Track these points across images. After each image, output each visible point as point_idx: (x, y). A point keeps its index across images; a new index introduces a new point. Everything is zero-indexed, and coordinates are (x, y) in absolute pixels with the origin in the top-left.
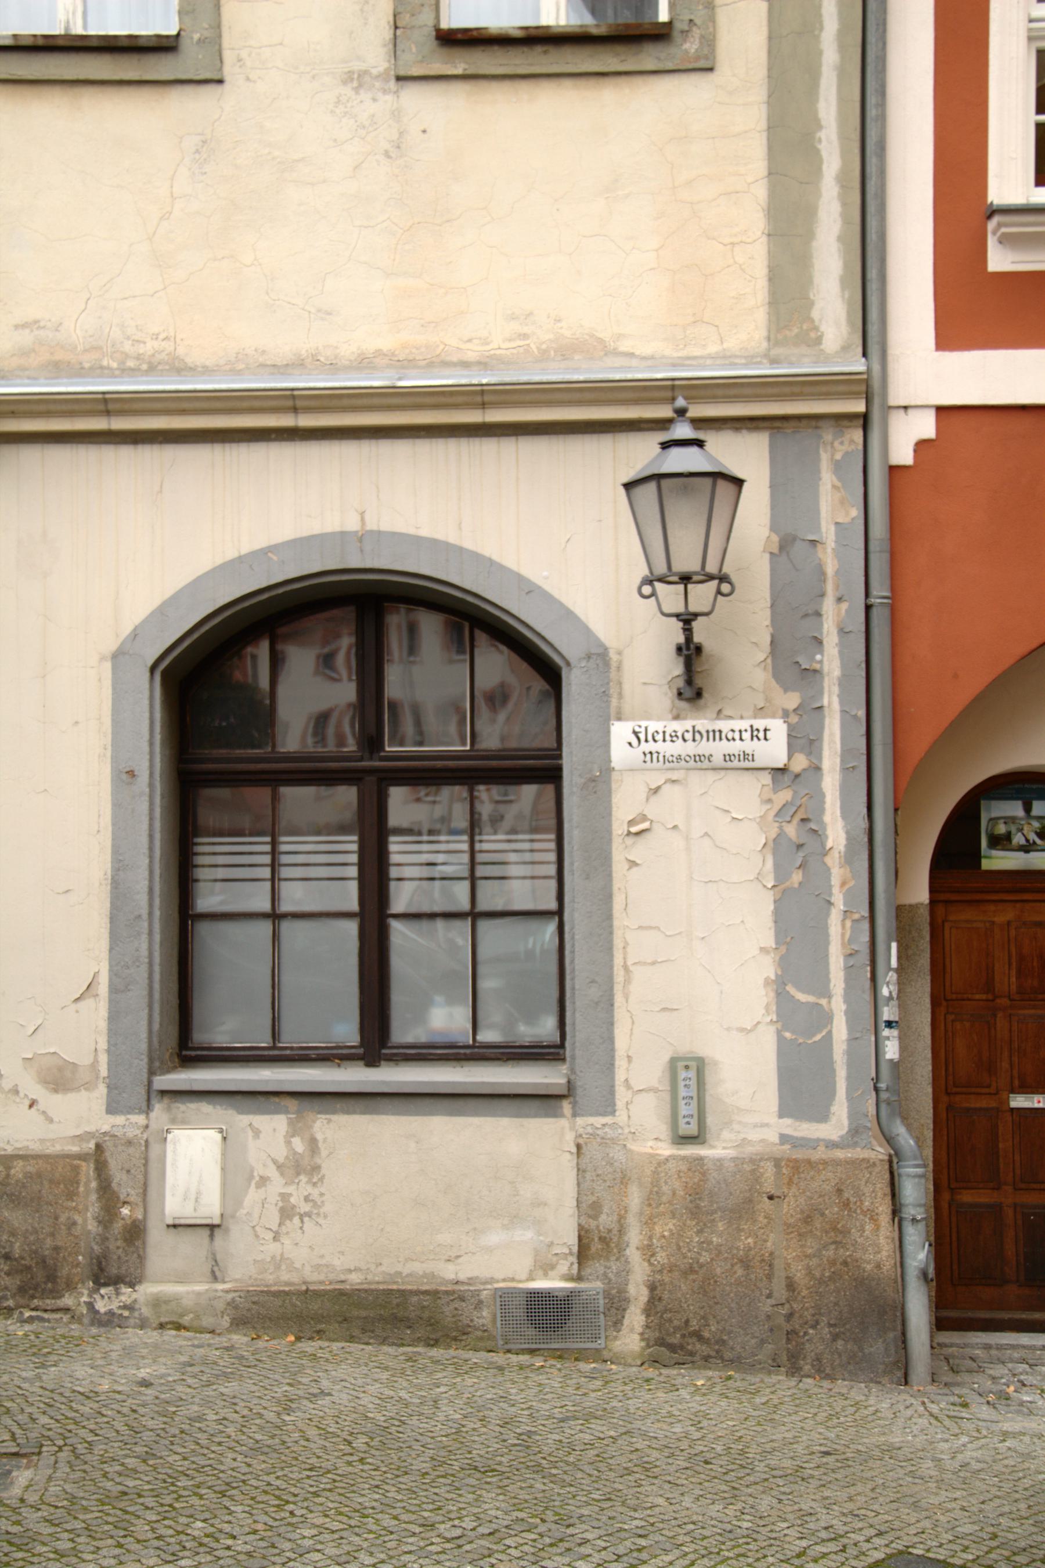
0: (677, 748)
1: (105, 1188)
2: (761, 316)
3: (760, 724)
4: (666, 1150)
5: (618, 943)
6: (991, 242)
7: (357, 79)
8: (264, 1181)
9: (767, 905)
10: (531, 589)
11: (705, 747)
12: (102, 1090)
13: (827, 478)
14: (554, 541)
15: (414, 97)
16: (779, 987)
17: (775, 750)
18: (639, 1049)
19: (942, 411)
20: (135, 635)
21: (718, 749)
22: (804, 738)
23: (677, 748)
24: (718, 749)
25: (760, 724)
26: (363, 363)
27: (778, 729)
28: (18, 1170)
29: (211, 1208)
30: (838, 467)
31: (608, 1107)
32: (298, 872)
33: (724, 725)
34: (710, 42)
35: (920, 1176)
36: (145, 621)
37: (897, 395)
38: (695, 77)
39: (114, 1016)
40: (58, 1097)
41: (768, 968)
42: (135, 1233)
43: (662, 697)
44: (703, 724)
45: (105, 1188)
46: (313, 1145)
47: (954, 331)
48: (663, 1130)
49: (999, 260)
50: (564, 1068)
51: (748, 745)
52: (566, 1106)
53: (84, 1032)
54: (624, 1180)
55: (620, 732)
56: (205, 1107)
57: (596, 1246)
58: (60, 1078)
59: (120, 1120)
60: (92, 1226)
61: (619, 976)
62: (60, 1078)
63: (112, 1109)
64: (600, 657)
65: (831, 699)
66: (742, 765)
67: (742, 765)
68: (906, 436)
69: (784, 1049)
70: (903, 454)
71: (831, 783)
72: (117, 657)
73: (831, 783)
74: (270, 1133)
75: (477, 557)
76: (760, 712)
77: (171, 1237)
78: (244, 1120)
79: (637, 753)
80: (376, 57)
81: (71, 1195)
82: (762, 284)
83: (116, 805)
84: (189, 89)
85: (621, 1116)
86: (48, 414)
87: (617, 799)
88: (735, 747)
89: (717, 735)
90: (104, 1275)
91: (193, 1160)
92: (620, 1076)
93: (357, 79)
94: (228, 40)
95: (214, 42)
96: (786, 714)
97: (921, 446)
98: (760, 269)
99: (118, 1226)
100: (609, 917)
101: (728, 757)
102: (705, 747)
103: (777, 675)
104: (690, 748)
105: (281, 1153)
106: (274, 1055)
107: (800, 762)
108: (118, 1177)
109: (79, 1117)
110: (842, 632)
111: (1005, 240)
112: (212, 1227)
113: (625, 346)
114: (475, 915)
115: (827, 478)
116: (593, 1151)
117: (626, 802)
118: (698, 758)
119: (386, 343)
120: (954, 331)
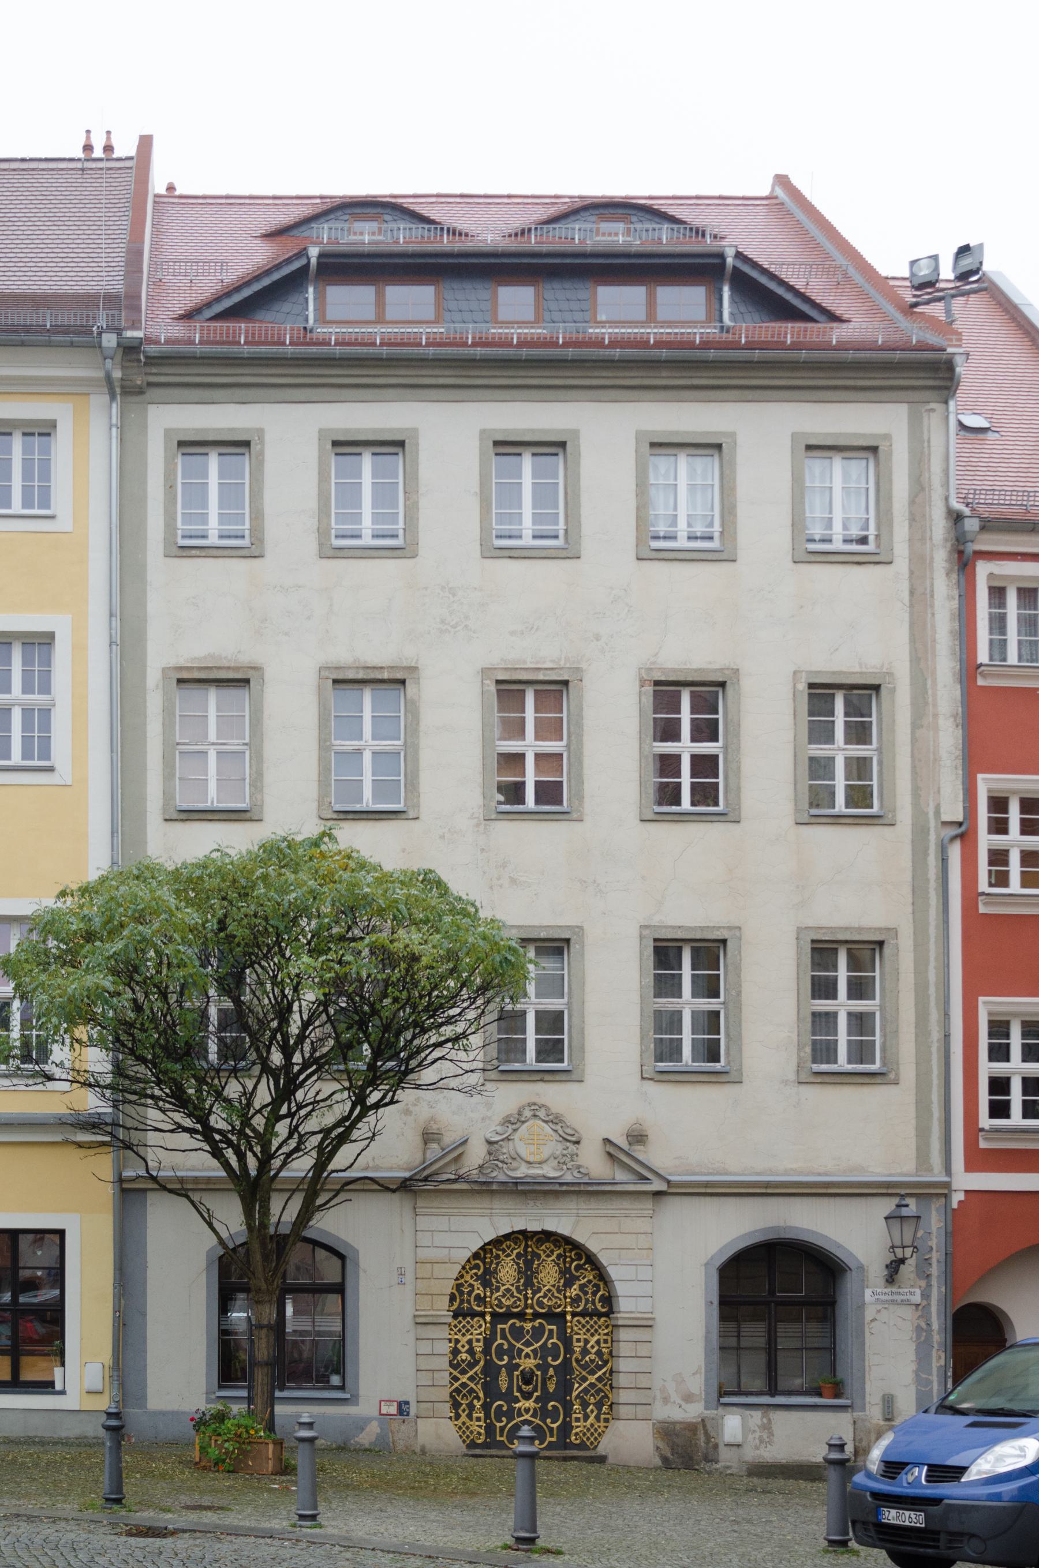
0: (886, 1297)
1: (706, 1433)
2: (914, 1161)
3: (912, 1290)
4: (882, 1423)
5: (867, 1358)
6: (980, 1139)
7: (785, 1082)
8: (754, 1431)
9: (913, 1346)
10: (839, 1246)
11: (895, 1297)
12: (703, 1403)
13: (934, 1213)
14: (856, 1235)
15: (803, 1087)
16: (917, 1373)
17: (917, 1298)
18: (873, 1393)
19: (966, 1191)
20: (712, 1258)
21: (899, 1298)
22: (926, 1296)
23: (886, 1297)
24: (899, 1298)
25: (912, 1290)
26: (786, 1173)
27: (918, 1291)
28: (678, 1427)
29: (739, 1439)
30: (937, 1210)
31: (863, 1409)
32: (783, 1334)
33: (901, 1290)
34: (897, 1075)
35: (619, 1312)
36: (716, 1254)
37: (954, 1187)
38: (893, 1086)
39: (706, 1380)
40: (689, 1405)
41: (913, 1367)
42: (716, 1446)
43: (882, 1281)
44: (894, 1290)
45: (706, 1433)
46: (769, 1420)
47: (971, 1166)
48: (880, 1417)
49: (983, 1145)
50: (440, 1432)
51: (909, 1297)
52: (850, 1410)
53: (697, 1384)
54: (870, 1432)
55: (868, 1293)
56: (735, 1409)
57: (861, 1452)
58: (689, 1398)
59: (709, 1412)
60: (703, 1444)
61: (867, 1369)
62: (689, 1398)
63: (706, 1408)
64: (861, 1268)
65: (934, 1282)
66: (907, 1303)
67: (907, 1303)
68: (957, 1197)
69: (918, 1392)
70: (955, 1205)
71: (934, 1309)
72: (706, 1264)
73: (934, 1309)
74: (756, 1417)
75: (823, 1236)
76: (912, 1286)
77: (726, 1448)
78: (748, 1412)
79: (873, 1299)
80: (792, 1076)
81: (695, 1435)
82: (914, 1151)
83: (706, 1313)
84: (731, 1085)
85: (868, 1412)
86: (682, 1187)
87: (866, 1313)
88: (904, 1297)
89: (899, 1293)
90: (707, 1459)
91: (733, 1425)
92: (867, 1399)
93: (785, 1082)
94: (744, 1070)
95: (740, 1071)
96: (920, 1287)
97: (960, 1202)
98: (914, 1146)
99: (711, 1445)
100: (864, 1350)
101: (902, 1301)
102: (895, 1297)
103: (917, 1275)
104: (890, 1298)
105: (759, 1423)
106: (739, 1393)
107: (925, 1303)
108: (710, 1429)
109: (693, 1412)
110: (938, 1261)
111: (986, 1139)
112: (739, 1445)
113: (871, 1169)
114: (738, 1348)
115: (934, 1213)
116: (859, 1424)
117: (869, 1313)
118: (893, 1301)
119: (794, 1166)
120: (971, 1166)
